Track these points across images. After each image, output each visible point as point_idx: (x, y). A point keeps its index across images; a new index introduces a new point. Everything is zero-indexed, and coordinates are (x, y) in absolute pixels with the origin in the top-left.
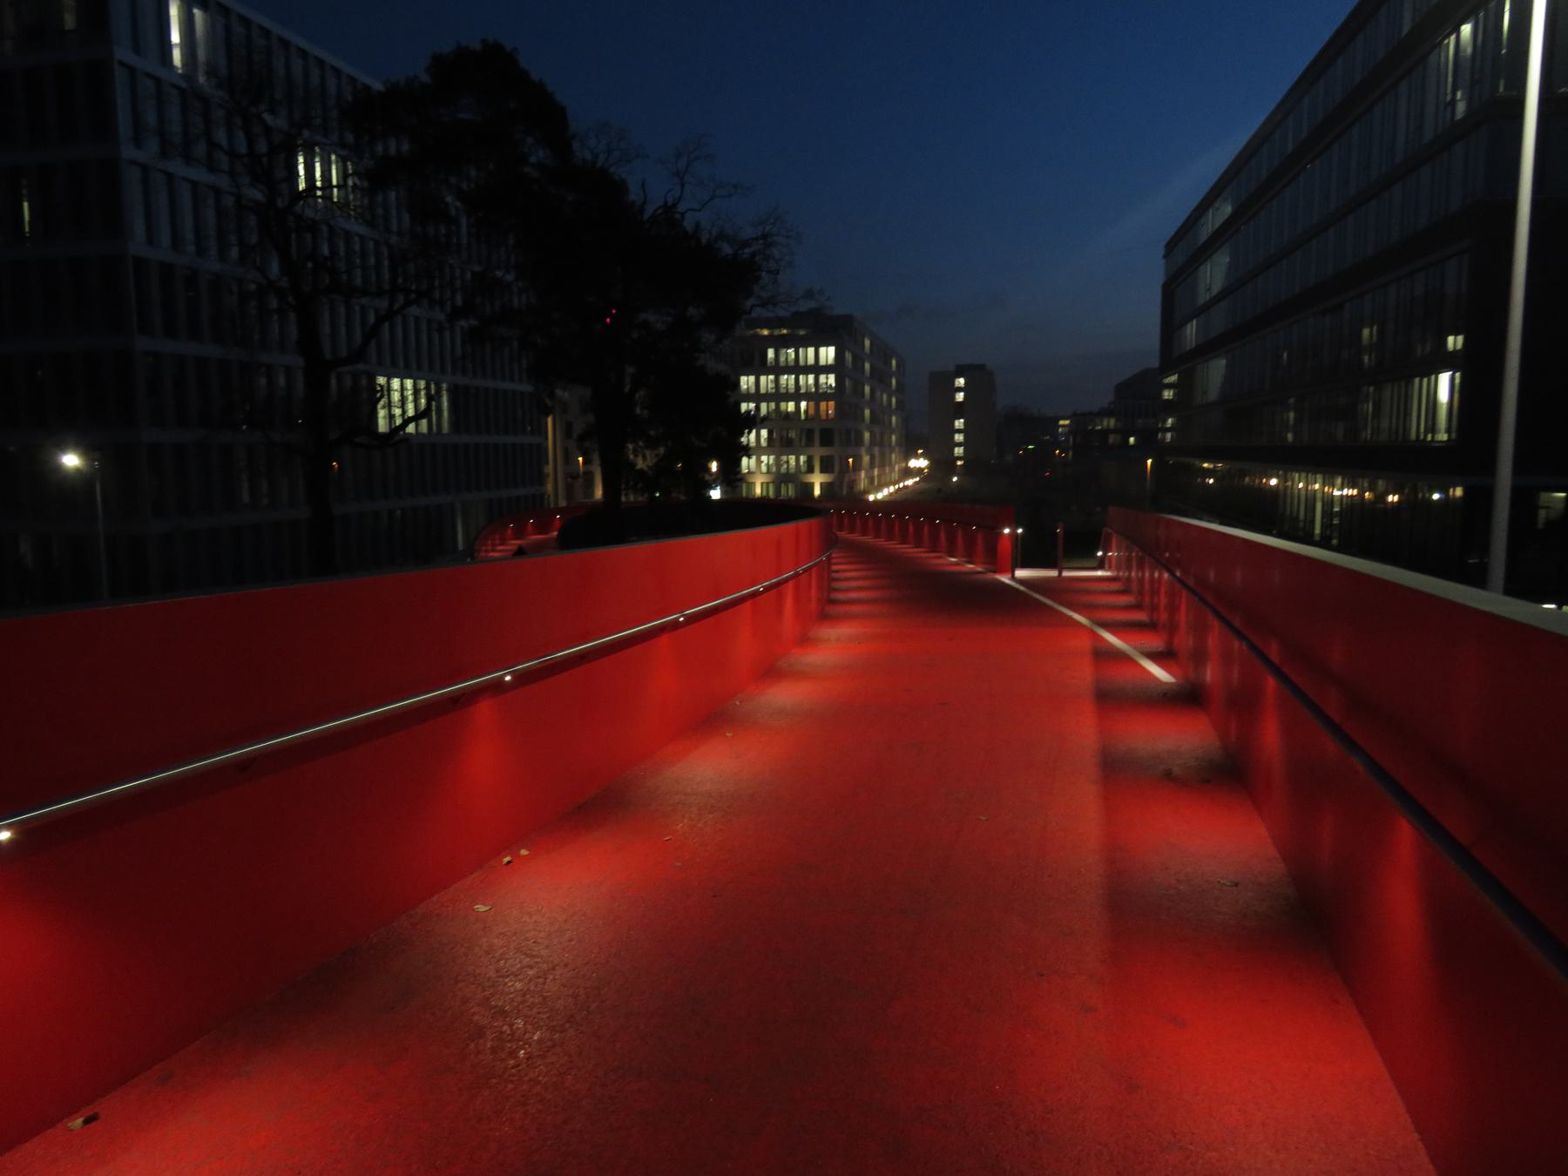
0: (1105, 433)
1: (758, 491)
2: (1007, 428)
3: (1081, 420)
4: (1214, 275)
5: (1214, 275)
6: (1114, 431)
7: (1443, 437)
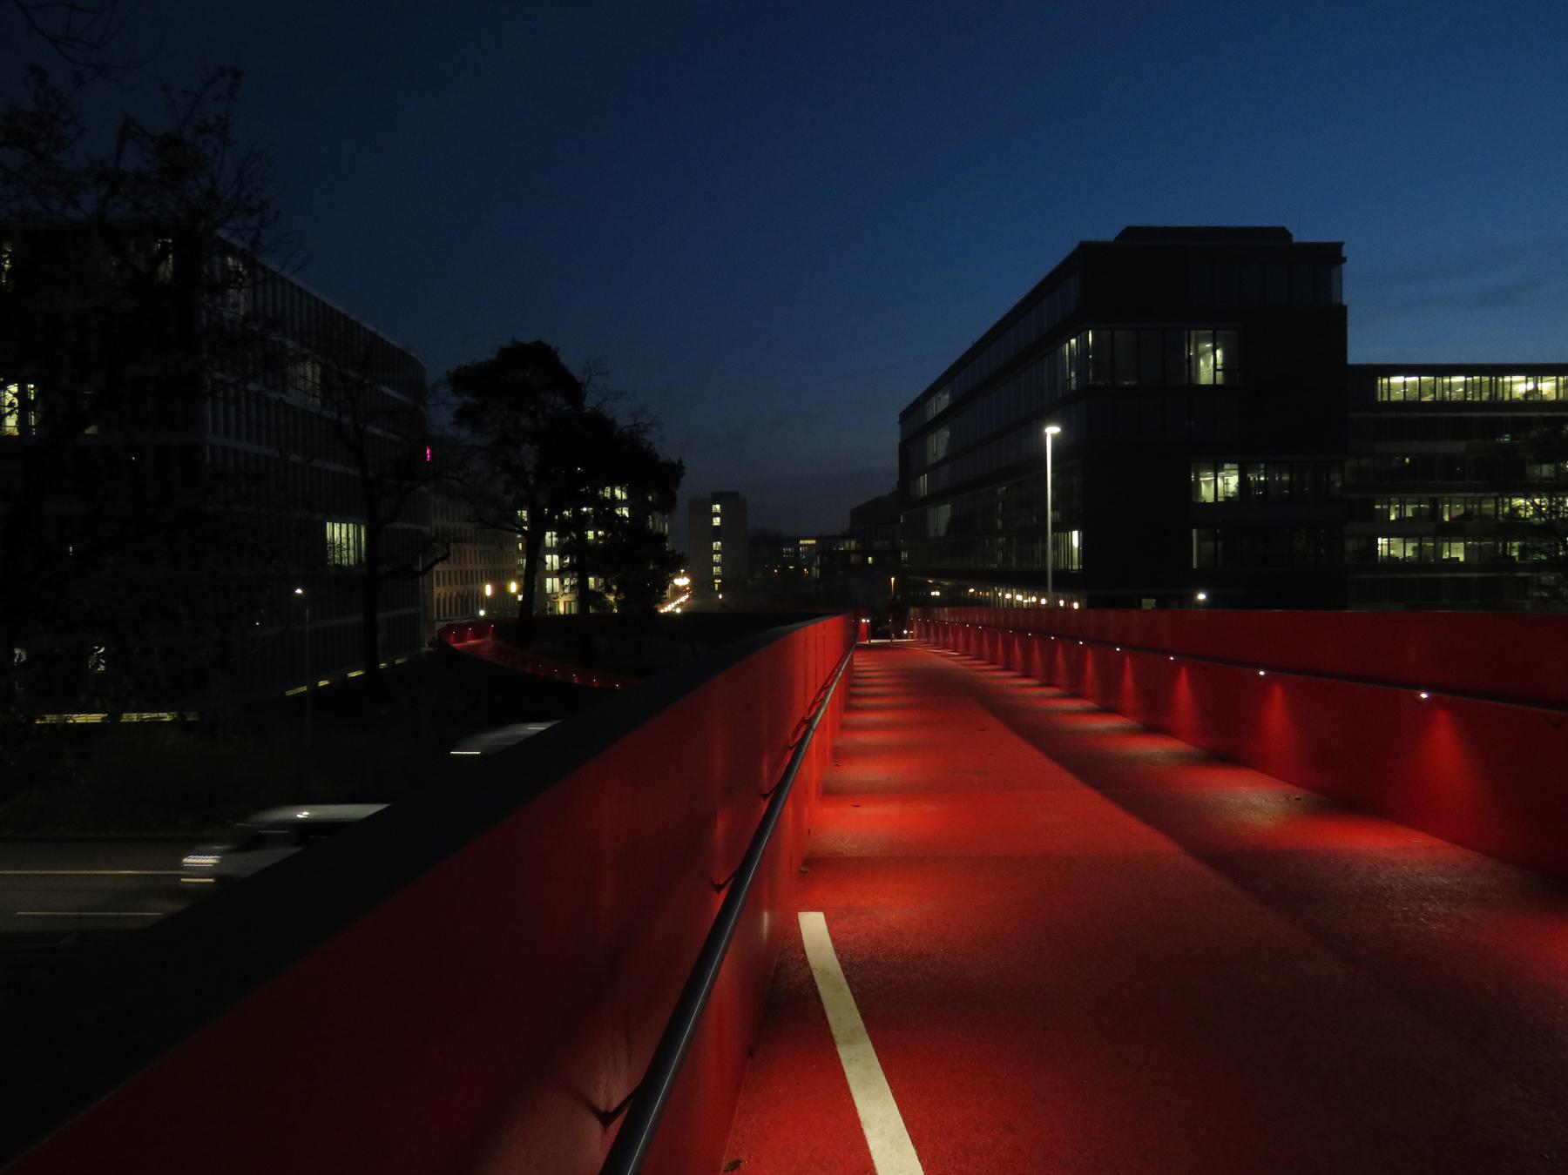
0: (848, 553)
1: (562, 609)
2: (757, 546)
3: (826, 543)
4: (938, 444)
5: (938, 444)
6: (856, 552)
7: (1076, 567)
